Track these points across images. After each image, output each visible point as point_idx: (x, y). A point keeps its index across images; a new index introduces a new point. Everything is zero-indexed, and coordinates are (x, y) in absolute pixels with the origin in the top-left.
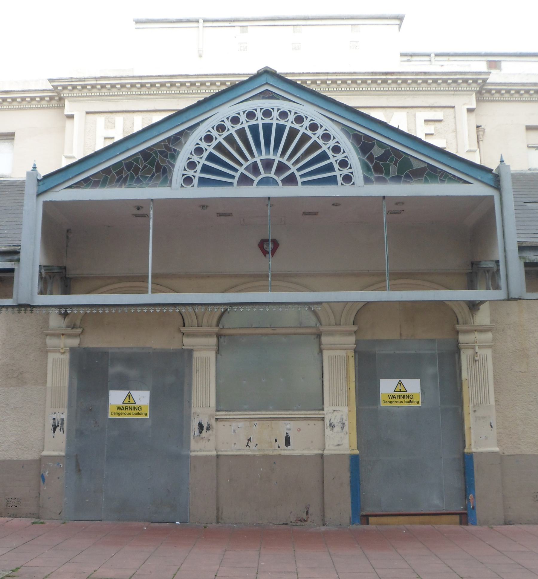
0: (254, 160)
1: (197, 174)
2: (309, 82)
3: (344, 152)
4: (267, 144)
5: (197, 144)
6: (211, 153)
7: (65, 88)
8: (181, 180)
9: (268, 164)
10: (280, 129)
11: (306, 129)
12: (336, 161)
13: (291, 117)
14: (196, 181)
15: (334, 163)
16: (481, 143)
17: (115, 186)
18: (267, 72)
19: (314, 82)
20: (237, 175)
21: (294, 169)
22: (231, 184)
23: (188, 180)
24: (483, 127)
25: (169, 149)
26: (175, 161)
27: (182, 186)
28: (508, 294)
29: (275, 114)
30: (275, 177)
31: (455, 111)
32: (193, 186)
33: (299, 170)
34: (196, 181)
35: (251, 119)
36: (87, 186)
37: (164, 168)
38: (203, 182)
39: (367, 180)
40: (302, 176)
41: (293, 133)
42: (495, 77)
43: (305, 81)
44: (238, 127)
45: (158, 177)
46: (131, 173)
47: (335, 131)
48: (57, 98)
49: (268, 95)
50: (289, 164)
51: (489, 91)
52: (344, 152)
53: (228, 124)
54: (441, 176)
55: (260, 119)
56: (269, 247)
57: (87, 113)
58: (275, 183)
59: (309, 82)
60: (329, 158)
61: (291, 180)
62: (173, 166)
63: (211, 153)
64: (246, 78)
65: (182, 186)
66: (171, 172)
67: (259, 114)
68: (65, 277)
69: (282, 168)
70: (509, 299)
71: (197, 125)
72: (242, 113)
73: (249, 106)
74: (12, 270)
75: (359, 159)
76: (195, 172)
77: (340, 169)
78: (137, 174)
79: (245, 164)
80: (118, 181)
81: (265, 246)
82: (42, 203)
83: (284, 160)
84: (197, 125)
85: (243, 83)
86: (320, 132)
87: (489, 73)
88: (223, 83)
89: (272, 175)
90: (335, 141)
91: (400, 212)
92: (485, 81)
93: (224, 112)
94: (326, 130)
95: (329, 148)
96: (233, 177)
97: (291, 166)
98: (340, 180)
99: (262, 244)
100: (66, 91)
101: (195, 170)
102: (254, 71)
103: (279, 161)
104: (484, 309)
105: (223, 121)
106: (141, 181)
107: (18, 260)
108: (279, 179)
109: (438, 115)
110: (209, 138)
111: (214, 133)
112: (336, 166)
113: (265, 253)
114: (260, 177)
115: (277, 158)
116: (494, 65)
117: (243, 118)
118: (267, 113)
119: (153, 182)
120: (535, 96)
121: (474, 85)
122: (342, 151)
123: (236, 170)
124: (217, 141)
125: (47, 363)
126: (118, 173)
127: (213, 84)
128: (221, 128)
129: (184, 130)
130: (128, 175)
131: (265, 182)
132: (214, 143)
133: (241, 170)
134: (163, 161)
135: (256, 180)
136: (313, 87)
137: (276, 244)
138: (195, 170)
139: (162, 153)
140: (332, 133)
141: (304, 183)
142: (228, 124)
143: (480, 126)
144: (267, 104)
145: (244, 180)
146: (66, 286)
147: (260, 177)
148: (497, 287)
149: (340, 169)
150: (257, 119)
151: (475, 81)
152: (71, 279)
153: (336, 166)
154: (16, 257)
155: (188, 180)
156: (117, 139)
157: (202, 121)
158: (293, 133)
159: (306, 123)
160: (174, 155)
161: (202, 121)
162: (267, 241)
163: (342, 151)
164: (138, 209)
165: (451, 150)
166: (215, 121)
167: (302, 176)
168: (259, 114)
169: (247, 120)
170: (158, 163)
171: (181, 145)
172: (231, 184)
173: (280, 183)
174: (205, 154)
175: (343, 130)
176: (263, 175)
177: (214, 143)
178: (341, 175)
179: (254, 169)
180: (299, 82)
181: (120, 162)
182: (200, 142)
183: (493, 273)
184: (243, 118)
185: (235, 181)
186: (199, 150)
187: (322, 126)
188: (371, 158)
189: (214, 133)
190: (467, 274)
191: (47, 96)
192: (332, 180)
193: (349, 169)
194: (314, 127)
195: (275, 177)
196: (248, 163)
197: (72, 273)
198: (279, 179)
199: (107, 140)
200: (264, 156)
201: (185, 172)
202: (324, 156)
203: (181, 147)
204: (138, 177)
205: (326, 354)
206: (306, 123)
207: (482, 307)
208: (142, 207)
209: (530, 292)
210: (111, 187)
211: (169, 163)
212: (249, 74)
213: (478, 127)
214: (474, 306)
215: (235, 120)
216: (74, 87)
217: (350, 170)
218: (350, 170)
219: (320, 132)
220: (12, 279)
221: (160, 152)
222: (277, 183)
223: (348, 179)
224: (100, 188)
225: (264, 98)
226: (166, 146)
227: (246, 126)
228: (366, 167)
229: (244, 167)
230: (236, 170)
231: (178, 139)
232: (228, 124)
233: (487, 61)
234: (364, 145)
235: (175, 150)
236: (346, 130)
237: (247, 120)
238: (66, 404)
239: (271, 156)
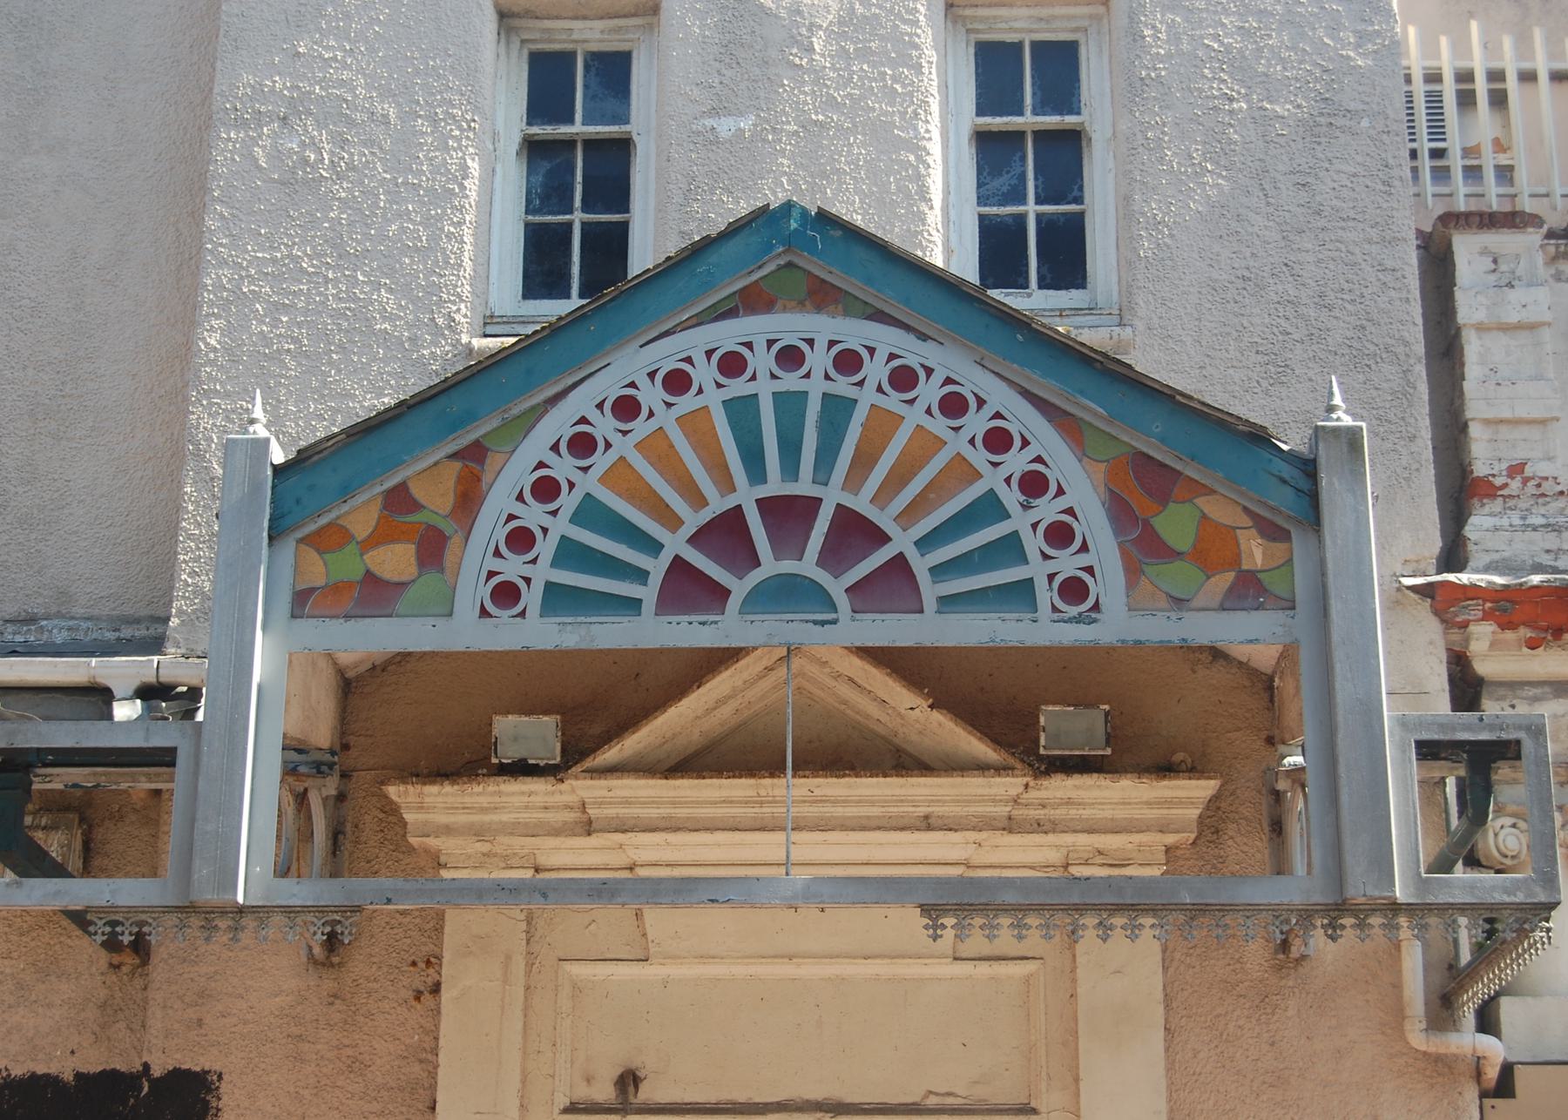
4: (790, 449)
5: (541, 465)
21: (902, 542)
23: (506, 594)
27: (484, 613)
30: (822, 577)
32: (522, 614)
35: (914, 387)
38: (558, 598)
60: (677, 559)
89: (808, 565)
103: (840, 507)
108: (836, 587)
114: (755, 577)
123: (654, 547)
166: (607, 384)
172: (634, 605)
173: (843, 602)
176: (770, 565)
185: (648, 594)
195: (822, 577)
209: (1084, 277)
238: (1475, 430)
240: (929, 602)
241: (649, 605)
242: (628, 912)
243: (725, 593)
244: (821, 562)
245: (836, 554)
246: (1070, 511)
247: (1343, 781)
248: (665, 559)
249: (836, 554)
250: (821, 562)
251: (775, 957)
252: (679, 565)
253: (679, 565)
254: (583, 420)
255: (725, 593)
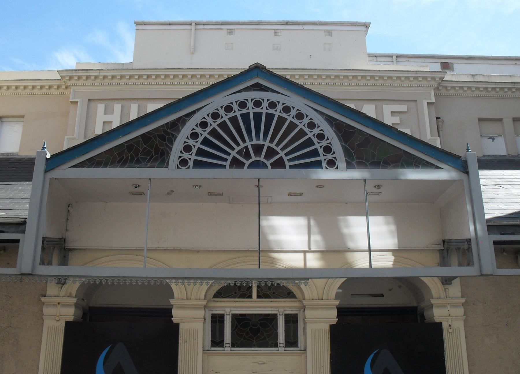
0: (245, 145)
2: (297, 77)
3: (328, 139)
6: (199, 149)
7: (71, 78)
8: (177, 162)
9: (258, 149)
10: (270, 117)
11: (293, 118)
12: (321, 147)
13: (280, 107)
14: (191, 163)
15: (319, 149)
16: (440, 132)
17: (117, 167)
18: (257, 69)
19: (301, 76)
20: (230, 158)
22: (224, 166)
23: (184, 163)
24: (441, 118)
25: (168, 134)
26: (172, 144)
27: (178, 167)
28: (481, 271)
29: (265, 104)
30: (265, 161)
31: (417, 105)
32: (189, 168)
33: (287, 154)
34: (191, 163)
36: (90, 166)
38: (198, 164)
40: (289, 160)
41: (281, 121)
43: (293, 76)
44: (231, 115)
45: (156, 160)
46: (131, 155)
47: (318, 120)
48: (64, 87)
49: (258, 87)
51: (446, 87)
52: (328, 139)
54: (415, 162)
55: (251, 108)
58: (265, 166)
59: (297, 77)
60: (315, 145)
62: (171, 149)
63: (199, 149)
64: (238, 72)
65: (178, 167)
66: (168, 155)
67: (250, 104)
68: (64, 249)
69: (271, 152)
71: (194, 112)
72: (234, 103)
73: (241, 97)
74: (18, 241)
75: (342, 145)
76: (191, 154)
77: (324, 154)
78: (137, 156)
79: (237, 149)
80: (119, 162)
84: (194, 112)
85: (236, 76)
86: (306, 121)
88: (220, 76)
89: (262, 159)
90: (320, 129)
91: (378, 194)
92: (442, 79)
93: (218, 101)
94: (311, 119)
95: (314, 135)
96: (226, 160)
97: (280, 151)
101: (190, 153)
102: (246, 66)
104: (456, 282)
105: (217, 109)
106: (141, 163)
107: (24, 232)
108: (268, 163)
109: (403, 108)
110: (204, 124)
111: (209, 120)
112: (321, 151)
114: (251, 161)
116: (446, 66)
117: (235, 107)
118: (257, 103)
119: (151, 163)
120: (518, 93)
122: (326, 138)
123: (229, 154)
124: (196, 148)
125: (42, 330)
126: (119, 154)
127: (211, 76)
128: (215, 116)
129: (181, 117)
130: (156, 140)
132: (209, 129)
133: (234, 153)
135: (247, 163)
136: (300, 82)
138: (190, 153)
139: (160, 136)
140: (316, 122)
141: (291, 167)
142: (222, 112)
143: (439, 118)
144: (257, 95)
145: (236, 163)
146: (65, 257)
147: (251, 161)
148: (470, 263)
149: (324, 154)
150: (248, 109)
153: (321, 151)
154: (21, 228)
155: (184, 163)
156: (114, 126)
157: (198, 110)
158: (281, 121)
159: (293, 113)
160: (172, 140)
161: (198, 110)
163: (326, 138)
165: (417, 136)
166: (210, 109)
167: (289, 160)
168: (250, 104)
169: (240, 109)
171: (179, 131)
173: (269, 166)
174: (200, 139)
176: (254, 158)
177: (209, 129)
178: (325, 160)
180: (288, 77)
181: (122, 145)
182: (195, 128)
183: (464, 250)
184: (235, 107)
185: (228, 164)
186: (194, 135)
189: (209, 120)
191: (55, 85)
193: (333, 154)
194: (300, 116)
195: (265, 161)
196: (240, 148)
197: (70, 245)
198: (268, 163)
200: (255, 142)
201: (181, 155)
202: (310, 143)
204: (138, 158)
205: (308, 325)
206: (293, 113)
207: (454, 282)
208: (139, 186)
210: (113, 167)
212: (241, 69)
213: (437, 118)
215: (228, 109)
216: (79, 78)
217: (334, 156)
218: (334, 156)
219: (306, 121)
220: (17, 248)
221: (159, 136)
222: (266, 166)
224: (103, 167)
225: (254, 90)
226: (165, 131)
227: (238, 114)
228: (347, 153)
229: (236, 151)
230: (229, 154)
231: (176, 126)
233: (441, 63)
234: (345, 133)
235: (173, 135)
236: (330, 120)
237: (240, 109)
239: (261, 142)
240: (287, 167)
241: (228, 166)
242: (365, 217)
243: (244, 164)
244: (265, 158)
245: (267, 157)
246: (189, 168)
247: (14, 244)
248: (231, 156)
249: (267, 157)
250: (265, 158)
251: (198, 251)
252: (234, 158)
253: (234, 158)
254: (193, 129)
255: (244, 164)
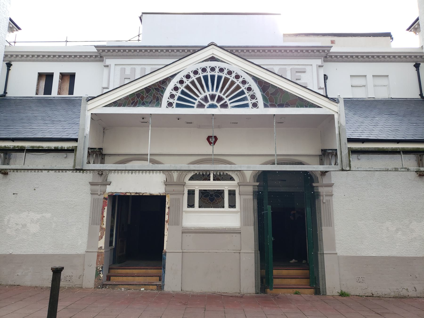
1: (175, 101)
14: (174, 105)
17: (131, 106)
22: (193, 107)
23: (170, 104)
26: (163, 94)
30: (217, 104)
34: (174, 105)
37: (158, 97)
38: (178, 105)
39: (266, 106)
42: (334, 49)
50: (224, 97)
53: (192, 75)
56: (212, 140)
57: (115, 65)
61: (225, 106)
62: (162, 96)
66: (161, 100)
70: (343, 170)
78: (142, 100)
81: (210, 140)
82: (59, 74)
83: (221, 95)
87: (331, 47)
89: (215, 102)
92: (329, 51)
96: (194, 103)
97: (225, 98)
98: (251, 105)
99: (208, 138)
100: (104, 53)
110: (181, 82)
113: (210, 143)
114: (208, 104)
115: (218, 94)
118: (213, 69)
121: (323, 53)
131: (212, 106)
132: (184, 85)
134: (157, 94)
135: (207, 105)
137: (216, 138)
144: (213, 64)
145: (201, 106)
147: (208, 104)
151: (324, 51)
152: (105, 155)
155: (170, 104)
160: (163, 91)
162: (212, 137)
164: (143, 118)
170: (154, 95)
171: (167, 86)
175: (253, 78)
176: (210, 102)
179: (205, 99)
185: (195, 106)
187: (242, 77)
188: (267, 94)
190: (319, 155)
192: (246, 105)
195: (217, 104)
198: (219, 105)
199: (126, 80)
203: (167, 87)
211: (160, 95)
214: (324, 173)
223: (255, 105)
228: (264, 98)
232: (192, 75)
235: (163, 88)
